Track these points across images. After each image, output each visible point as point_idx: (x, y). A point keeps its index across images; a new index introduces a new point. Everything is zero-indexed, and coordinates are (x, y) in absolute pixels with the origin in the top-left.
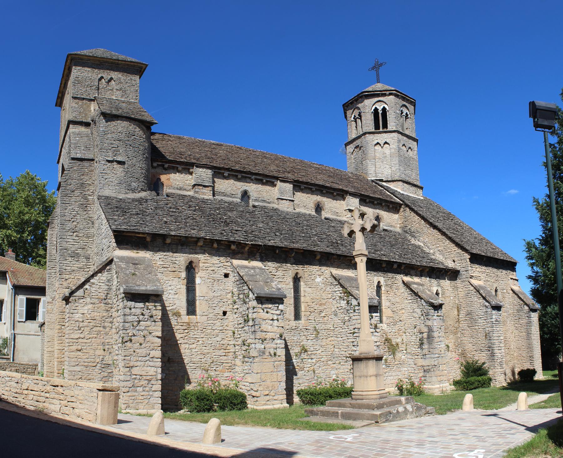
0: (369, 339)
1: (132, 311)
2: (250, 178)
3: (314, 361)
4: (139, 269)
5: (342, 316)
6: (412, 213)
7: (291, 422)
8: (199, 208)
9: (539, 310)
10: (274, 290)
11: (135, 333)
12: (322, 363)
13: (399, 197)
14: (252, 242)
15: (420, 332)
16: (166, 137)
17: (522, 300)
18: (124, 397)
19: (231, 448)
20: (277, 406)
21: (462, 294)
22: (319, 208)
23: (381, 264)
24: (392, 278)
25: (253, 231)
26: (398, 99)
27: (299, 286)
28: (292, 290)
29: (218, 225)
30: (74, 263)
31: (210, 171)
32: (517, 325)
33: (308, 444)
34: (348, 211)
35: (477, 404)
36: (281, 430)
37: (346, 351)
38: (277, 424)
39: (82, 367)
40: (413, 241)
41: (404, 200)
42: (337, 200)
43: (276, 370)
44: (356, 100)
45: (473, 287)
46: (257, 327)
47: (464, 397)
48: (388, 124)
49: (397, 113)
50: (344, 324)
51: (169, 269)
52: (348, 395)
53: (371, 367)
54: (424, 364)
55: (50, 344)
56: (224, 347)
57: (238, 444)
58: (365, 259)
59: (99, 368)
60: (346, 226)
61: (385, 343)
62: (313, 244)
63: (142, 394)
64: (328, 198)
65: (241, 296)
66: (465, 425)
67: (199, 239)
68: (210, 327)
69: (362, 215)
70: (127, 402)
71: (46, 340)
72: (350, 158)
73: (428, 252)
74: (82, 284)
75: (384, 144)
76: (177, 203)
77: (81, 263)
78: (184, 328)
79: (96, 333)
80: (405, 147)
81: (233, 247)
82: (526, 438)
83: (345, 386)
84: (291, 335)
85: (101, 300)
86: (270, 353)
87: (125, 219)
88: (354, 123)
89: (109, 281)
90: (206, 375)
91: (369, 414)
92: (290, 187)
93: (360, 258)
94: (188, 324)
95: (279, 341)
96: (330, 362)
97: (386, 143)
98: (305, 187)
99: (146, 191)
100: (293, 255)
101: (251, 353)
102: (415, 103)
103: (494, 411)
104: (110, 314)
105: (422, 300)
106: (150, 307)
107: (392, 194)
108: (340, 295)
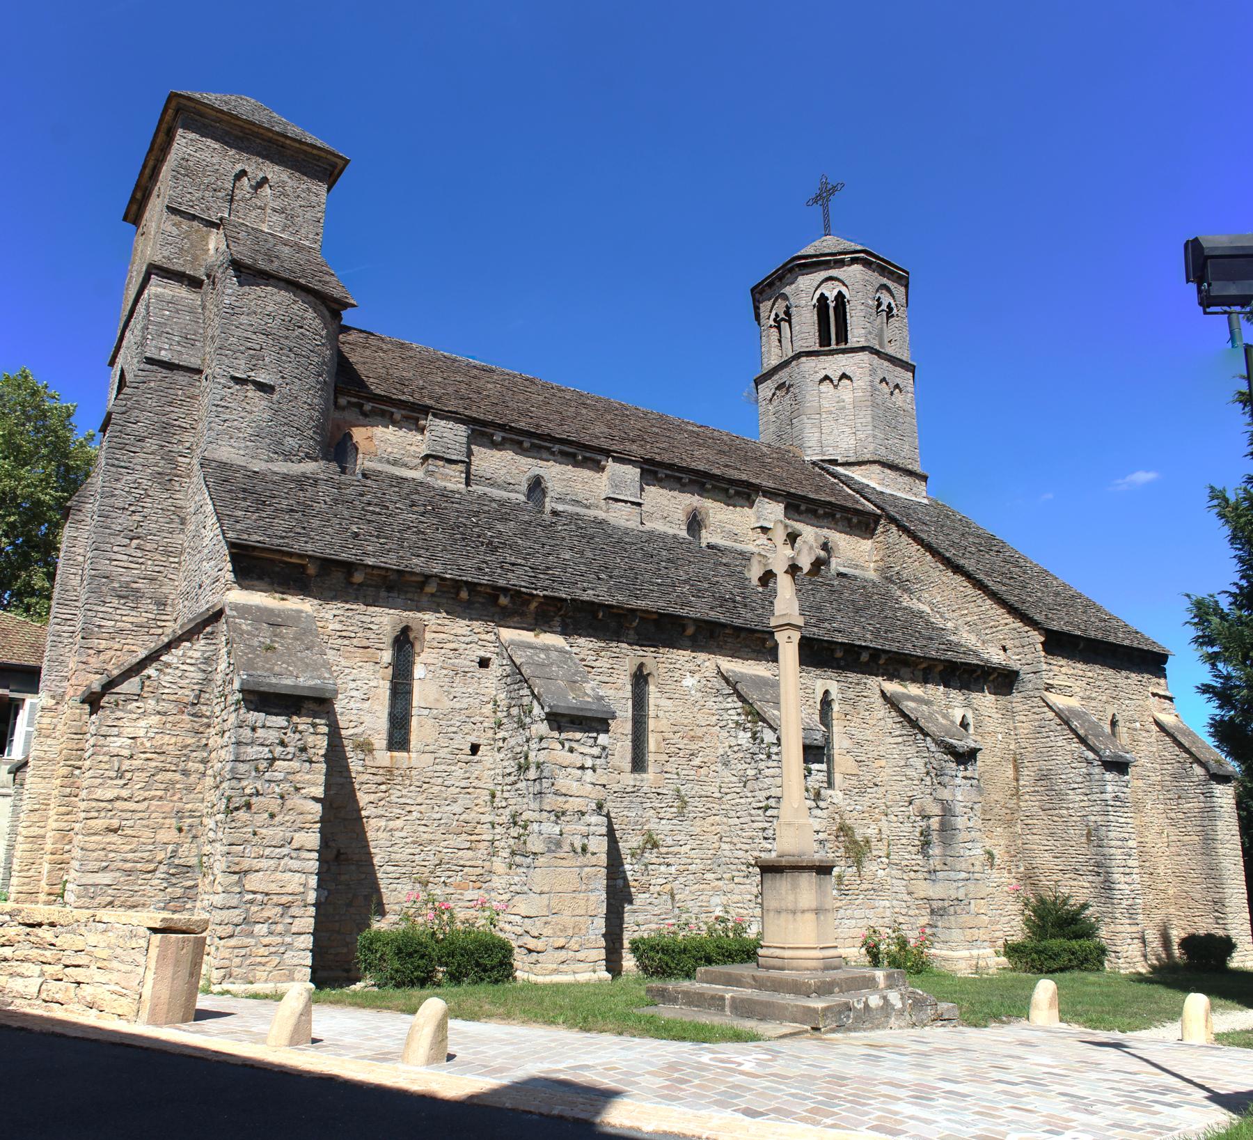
0: (802, 821)
1: (256, 735)
2: (548, 449)
3: (673, 869)
4: (283, 638)
5: (740, 767)
7: (614, 1016)
8: (433, 509)
9: (1237, 779)
10: (590, 700)
11: (259, 788)
12: (691, 877)
14: (545, 592)
15: (923, 813)
16: (372, 341)
17: (1187, 751)
18: (221, 949)
19: (468, 1076)
20: (583, 977)
21: (1025, 729)
22: (695, 523)
23: (833, 651)
24: (858, 684)
25: (548, 568)
27: (644, 694)
28: (630, 703)
29: (473, 551)
30: (124, 613)
31: (463, 427)
32: (1173, 815)
33: (649, 1073)
35: (1069, 1010)
36: (588, 1035)
37: (747, 851)
38: (579, 1019)
39: (118, 874)
40: (906, 601)
41: (884, 506)
42: (735, 506)
43: (584, 887)
45: (1054, 711)
46: (546, 783)
47: (1032, 988)
50: (745, 787)
51: (355, 642)
52: (749, 958)
53: (805, 890)
54: (931, 894)
55: (35, 817)
56: (468, 828)
57: (485, 1067)
58: (796, 636)
59: (162, 876)
60: (755, 561)
61: (837, 837)
62: (679, 600)
63: (266, 941)
65: (514, 711)
66: (1038, 1061)
67: (428, 577)
68: (440, 780)
69: (792, 538)
70: (227, 963)
71: (26, 805)
72: (766, 412)
73: (941, 626)
74: (138, 663)
75: (840, 380)
76: (384, 494)
77: (143, 614)
78: (379, 779)
79: (163, 786)
80: (887, 384)
81: (503, 601)
82: (1211, 1122)
83: (745, 935)
84: (623, 805)
85: (183, 706)
86: (572, 845)
87: (261, 518)
89: (207, 661)
90: (423, 896)
91: (797, 1006)
92: (633, 473)
93: (787, 633)
94: (390, 770)
95: (594, 819)
96: (709, 876)
97: (844, 376)
98: (667, 476)
99: (317, 461)
100: (635, 624)
101: (529, 845)
103: (1116, 1036)
104: (204, 741)
105: (928, 738)
106: (301, 728)
108: (736, 718)
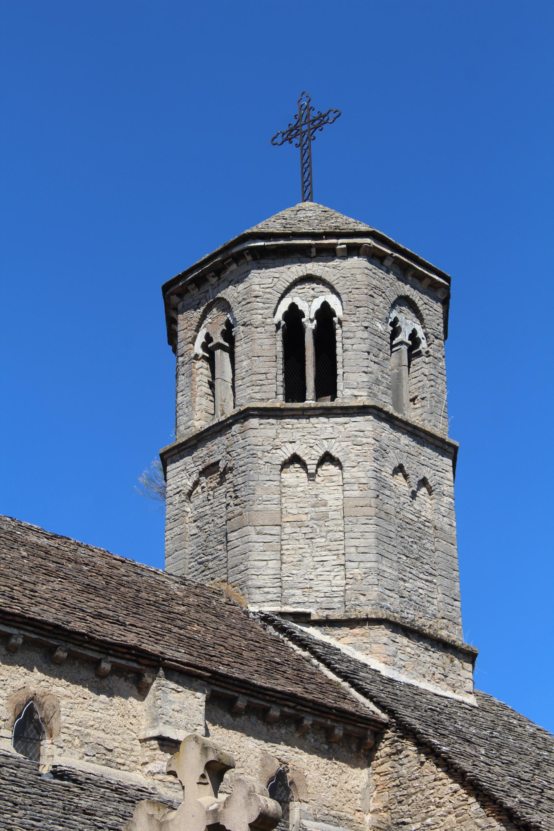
6: (430, 767)
13: (374, 692)
26: (380, 273)
34: (155, 743)
41: (394, 706)
42: (110, 694)
44: (219, 270)
48: (339, 379)
49: (375, 333)
64: (74, 681)
80: (406, 476)
88: (202, 366)
102: (448, 288)
107: (346, 678)
